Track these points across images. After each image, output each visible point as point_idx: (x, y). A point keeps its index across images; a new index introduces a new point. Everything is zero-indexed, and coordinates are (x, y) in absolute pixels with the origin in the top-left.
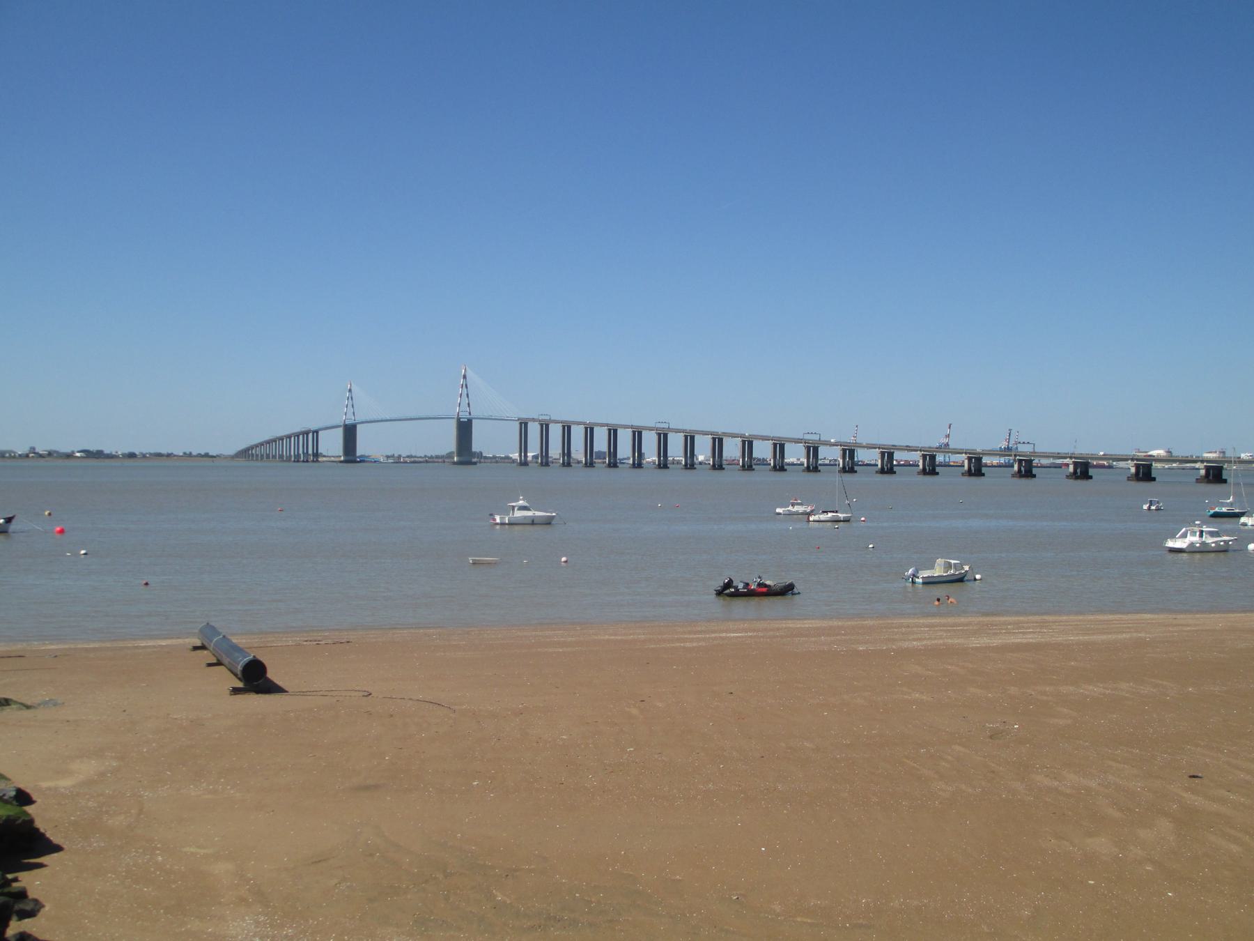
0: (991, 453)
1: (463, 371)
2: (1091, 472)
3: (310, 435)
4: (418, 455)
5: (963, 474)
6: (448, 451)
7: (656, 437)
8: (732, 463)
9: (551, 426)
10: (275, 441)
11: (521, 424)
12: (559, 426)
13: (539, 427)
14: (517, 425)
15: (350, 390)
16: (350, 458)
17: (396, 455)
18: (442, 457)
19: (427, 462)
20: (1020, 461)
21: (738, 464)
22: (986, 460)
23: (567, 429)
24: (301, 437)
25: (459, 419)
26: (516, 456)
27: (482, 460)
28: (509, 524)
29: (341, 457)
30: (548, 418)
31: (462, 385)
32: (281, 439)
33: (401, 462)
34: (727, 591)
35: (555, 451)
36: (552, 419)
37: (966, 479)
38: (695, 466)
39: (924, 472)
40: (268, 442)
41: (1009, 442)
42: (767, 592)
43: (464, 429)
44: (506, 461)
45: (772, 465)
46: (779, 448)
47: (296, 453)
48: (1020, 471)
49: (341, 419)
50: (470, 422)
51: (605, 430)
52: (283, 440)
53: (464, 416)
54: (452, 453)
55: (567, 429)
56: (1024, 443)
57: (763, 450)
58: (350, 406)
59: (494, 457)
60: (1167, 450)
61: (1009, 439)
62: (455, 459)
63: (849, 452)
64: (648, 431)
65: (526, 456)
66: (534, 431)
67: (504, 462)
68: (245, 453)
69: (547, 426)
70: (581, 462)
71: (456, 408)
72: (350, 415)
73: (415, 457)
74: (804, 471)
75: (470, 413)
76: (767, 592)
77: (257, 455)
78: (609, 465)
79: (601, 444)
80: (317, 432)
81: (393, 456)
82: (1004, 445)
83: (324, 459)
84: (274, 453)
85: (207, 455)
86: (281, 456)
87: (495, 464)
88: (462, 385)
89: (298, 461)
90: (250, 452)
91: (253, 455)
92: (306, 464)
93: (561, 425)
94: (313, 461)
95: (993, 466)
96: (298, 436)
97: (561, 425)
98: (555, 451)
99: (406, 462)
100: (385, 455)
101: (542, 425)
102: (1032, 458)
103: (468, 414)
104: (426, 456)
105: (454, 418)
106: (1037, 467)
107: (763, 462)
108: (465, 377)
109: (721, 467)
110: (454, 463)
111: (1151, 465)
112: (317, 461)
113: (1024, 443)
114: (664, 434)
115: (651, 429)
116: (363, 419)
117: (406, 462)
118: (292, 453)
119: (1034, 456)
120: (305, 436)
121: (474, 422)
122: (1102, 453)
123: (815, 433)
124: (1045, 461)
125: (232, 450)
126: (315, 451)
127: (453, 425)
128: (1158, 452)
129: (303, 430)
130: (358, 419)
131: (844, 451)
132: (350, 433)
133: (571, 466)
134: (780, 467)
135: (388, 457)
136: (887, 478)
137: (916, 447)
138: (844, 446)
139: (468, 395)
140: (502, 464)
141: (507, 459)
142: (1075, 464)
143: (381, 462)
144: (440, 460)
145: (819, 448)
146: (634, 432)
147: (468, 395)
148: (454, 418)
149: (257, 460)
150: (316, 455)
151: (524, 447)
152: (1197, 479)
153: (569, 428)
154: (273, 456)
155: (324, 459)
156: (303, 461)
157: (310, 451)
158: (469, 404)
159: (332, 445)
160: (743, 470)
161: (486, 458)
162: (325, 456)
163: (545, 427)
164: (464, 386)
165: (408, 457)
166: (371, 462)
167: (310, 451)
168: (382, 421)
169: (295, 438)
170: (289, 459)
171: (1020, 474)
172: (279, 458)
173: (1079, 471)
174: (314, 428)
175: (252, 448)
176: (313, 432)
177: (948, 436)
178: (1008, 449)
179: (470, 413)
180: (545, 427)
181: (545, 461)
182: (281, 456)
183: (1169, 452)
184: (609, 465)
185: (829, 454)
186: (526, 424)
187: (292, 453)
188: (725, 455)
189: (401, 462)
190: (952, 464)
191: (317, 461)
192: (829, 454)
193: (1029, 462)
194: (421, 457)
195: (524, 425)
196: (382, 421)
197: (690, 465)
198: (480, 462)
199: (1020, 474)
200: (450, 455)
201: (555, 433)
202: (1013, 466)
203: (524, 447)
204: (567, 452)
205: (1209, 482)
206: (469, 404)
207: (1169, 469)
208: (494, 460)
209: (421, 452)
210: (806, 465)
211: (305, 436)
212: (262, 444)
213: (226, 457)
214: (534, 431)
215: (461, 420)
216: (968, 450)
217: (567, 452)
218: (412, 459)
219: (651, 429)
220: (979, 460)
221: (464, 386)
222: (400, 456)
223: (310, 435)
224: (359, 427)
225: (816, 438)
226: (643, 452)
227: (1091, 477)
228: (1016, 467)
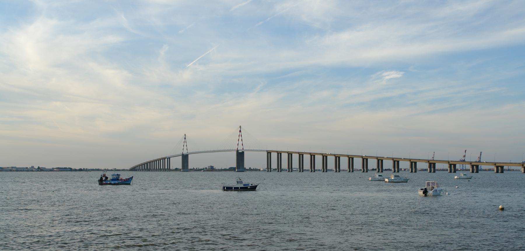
3: (166, 160)
14: (266, 153)
24: (162, 160)
25: (238, 151)
28: (459, 179)
31: (184, 142)
34: (481, 152)
35: (285, 165)
42: (481, 154)
43: (240, 156)
49: (180, 152)
50: (243, 153)
52: (156, 161)
53: (185, 152)
61: (480, 157)
76: (481, 154)
80: (169, 158)
88: (184, 142)
121: (245, 152)
125: (128, 168)
127: (235, 154)
128: (364, 155)
132: (185, 158)
159: (177, 163)
164: (185, 142)
169: (163, 161)
174: (168, 155)
176: (168, 158)
177: (465, 156)
181: (280, 169)
206: (187, 149)
215: (239, 152)
216: (159, 159)
221: (185, 142)
223: (166, 160)
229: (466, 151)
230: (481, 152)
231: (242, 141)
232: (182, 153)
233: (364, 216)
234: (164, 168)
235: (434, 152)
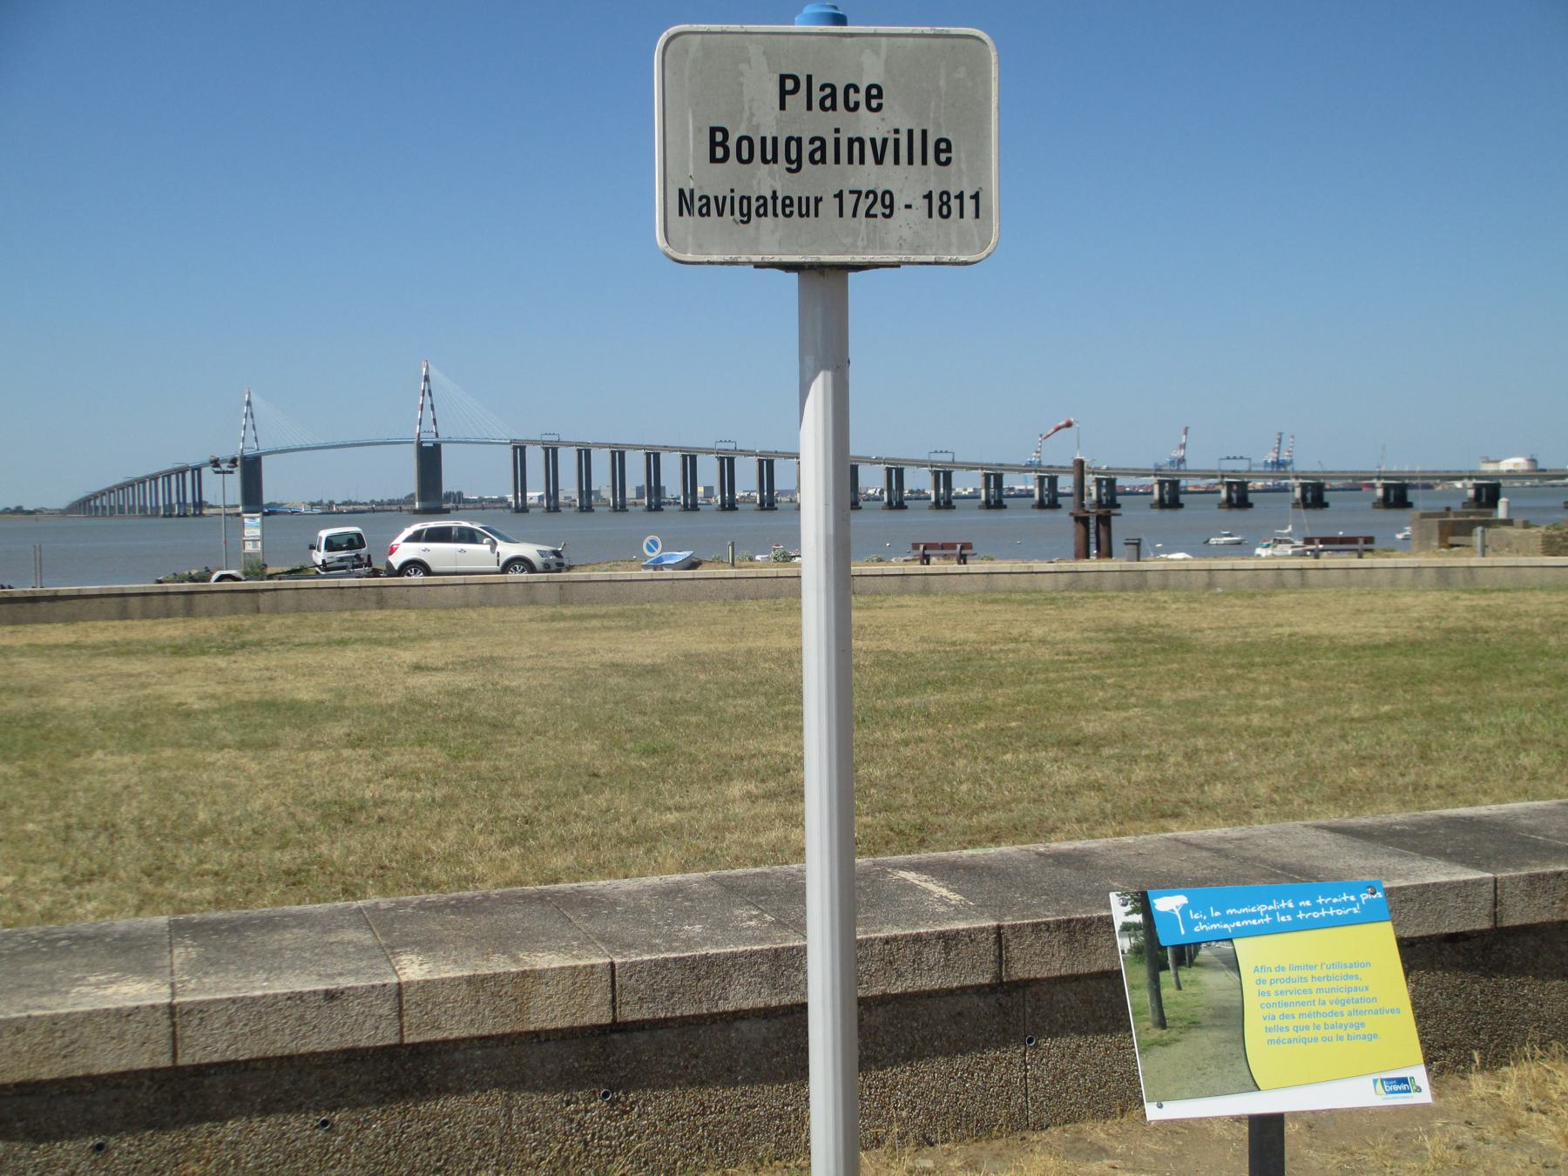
0: (1127, 473)
1: (424, 370)
2: (1327, 496)
4: (361, 500)
5: (1033, 507)
6: (408, 493)
7: (717, 463)
8: (748, 499)
9: (561, 451)
10: (133, 486)
11: (515, 448)
12: (641, 454)
13: (542, 453)
14: (509, 450)
15: (249, 403)
16: (431, 504)
17: (326, 501)
18: (399, 502)
19: (374, 511)
20: (1229, 485)
21: (755, 502)
22: (1121, 482)
23: (584, 456)
24: (174, 477)
25: (420, 444)
26: (510, 497)
27: (461, 506)
29: (237, 506)
30: (555, 438)
31: (424, 391)
32: (142, 481)
33: (334, 513)
35: (569, 488)
36: (563, 438)
37: (1156, 512)
38: (776, 505)
39: (1161, 504)
40: (122, 487)
41: (1278, 453)
43: (429, 459)
44: (498, 505)
45: (886, 500)
46: (943, 477)
47: (167, 503)
48: (1229, 499)
51: (676, 458)
53: (429, 439)
54: (412, 495)
55: (584, 456)
56: (1235, 458)
57: (918, 480)
58: (249, 427)
59: (481, 500)
60: (1529, 457)
61: (1279, 448)
62: (417, 505)
63: (994, 478)
64: (632, 451)
65: (524, 497)
66: (535, 458)
67: (495, 508)
68: (84, 506)
69: (555, 451)
70: (929, 498)
71: (414, 428)
72: (251, 442)
73: (355, 503)
74: (931, 508)
75: (437, 434)
76: (1280, 440)
77: (104, 508)
78: (649, 508)
79: (636, 476)
81: (320, 503)
82: (1271, 457)
83: (212, 511)
84: (121, 503)
85: (19, 510)
86: (143, 509)
87: (481, 511)
88: (424, 391)
89: (171, 516)
90: (92, 503)
91: (96, 508)
92: (169, 520)
93: (575, 448)
94: (194, 515)
95: (965, 497)
96: (169, 477)
97: (575, 448)
98: (569, 488)
99: (341, 513)
100: (307, 501)
101: (546, 450)
102: (1246, 480)
103: (434, 435)
104: (373, 502)
105: (412, 442)
106: (1009, 496)
107: (919, 495)
108: (427, 379)
109: (901, 506)
110: (416, 512)
111: (1178, 481)
112: (201, 514)
113: (1235, 458)
114: (768, 461)
115: (708, 452)
116: (271, 447)
117: (341, 513)
118: (161, 503)
119: (1248, 477)
120: (180, 475)
122: (1104, 467)
123: (1241, 458)
124: (1335, 483)
125: (63, 502)
126: (181, 500)
129: (177, 466)
130: (264, 447)
131: (987, 477)
132: (251, 469)
133: (593, 511)
134: (945, 503)
135: (312, 505)
136: (994, 515)
137: (1371, 472)
138: (986, 469)
139: (432, 406)
140: (492, 511)
141: (503, 500)
142: (1304, 487)
143: (302, 514)
144: (394, 508)
145: (953, 474)
146: (684, 457)
147: (432, 406)
148: (412, 442)
149: (104, 515)
150: (199, 505)
151: (520, 484)
152: (1464, 503)
153: (622, 455)
154: (129, 509)
155: (212, 511)
156: (179, 516)
157: (189, 500)
158: (434, 420)
160: (762, 510)
161: (467, 501)
162: (211, 507)
163: (551, 453)
165: (345, 503)
166: (286, 513)
167: (189, 500)
168: (301, 449)
169: (177, 477)
170: (169, 514)
171: (1229, 504)
172: (140, 512)
173: (1234, 495)
174: (193, 463)
175: (95, 497)
178: (1278, 464)
179: (437, 434)
180: (551, 453)
182: (143, 509)
183: (1533, 461)
184: (649, 508)
185: (966, 484)
186: (523, 449)
187: (161, 503)
188: (778, 486)
189: (334, 513)
190: (1190, 489)
191: (201, 514)
192: (966, 484)
193: (1243, 486)
194: (365, 504)
195: (519, 450)
196: (301, 449)
197: (691, 506)
198: (457, 509)
199: (1229, 504)
200: (409, 499)
201: (568, 462)
202: (1219, 492)
203: (520, 484)
204: (586, 491)
205: (1306, 506)
206: (434, 420)
207: (1531, 486)
208: (478, 505)
209: (365, 496)
210: (933, 499)
211: (180, 475)
212: (111, 491)
213: (52, 513)
214: (535, 458)
217: (586, 491)
218: (351, 508)
219: (708, 452)
220: (1111, 483)
222: (331, 503)
224: (265, 460)
225: (947, 458)
226: (662, 484)
227: (1326, 505)
228: (1224, 494)
229: (1186, 429)
230: (1280, 434)
231: (254, 429)
232: (239, 452)
233: (304, 640)
234: (181, 500)
235: (1186, 431)
